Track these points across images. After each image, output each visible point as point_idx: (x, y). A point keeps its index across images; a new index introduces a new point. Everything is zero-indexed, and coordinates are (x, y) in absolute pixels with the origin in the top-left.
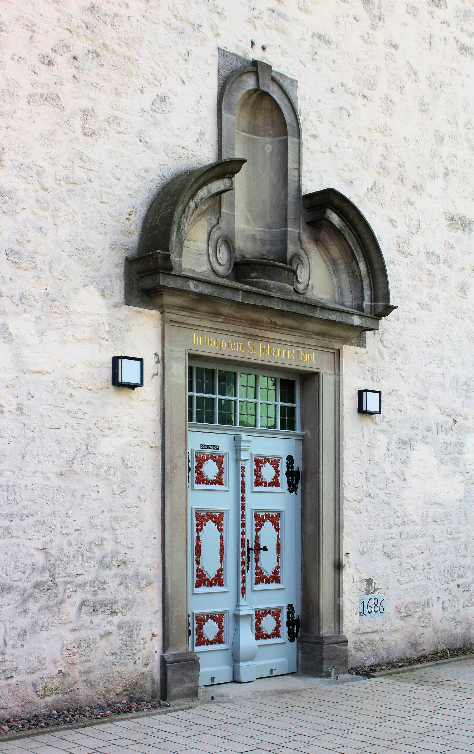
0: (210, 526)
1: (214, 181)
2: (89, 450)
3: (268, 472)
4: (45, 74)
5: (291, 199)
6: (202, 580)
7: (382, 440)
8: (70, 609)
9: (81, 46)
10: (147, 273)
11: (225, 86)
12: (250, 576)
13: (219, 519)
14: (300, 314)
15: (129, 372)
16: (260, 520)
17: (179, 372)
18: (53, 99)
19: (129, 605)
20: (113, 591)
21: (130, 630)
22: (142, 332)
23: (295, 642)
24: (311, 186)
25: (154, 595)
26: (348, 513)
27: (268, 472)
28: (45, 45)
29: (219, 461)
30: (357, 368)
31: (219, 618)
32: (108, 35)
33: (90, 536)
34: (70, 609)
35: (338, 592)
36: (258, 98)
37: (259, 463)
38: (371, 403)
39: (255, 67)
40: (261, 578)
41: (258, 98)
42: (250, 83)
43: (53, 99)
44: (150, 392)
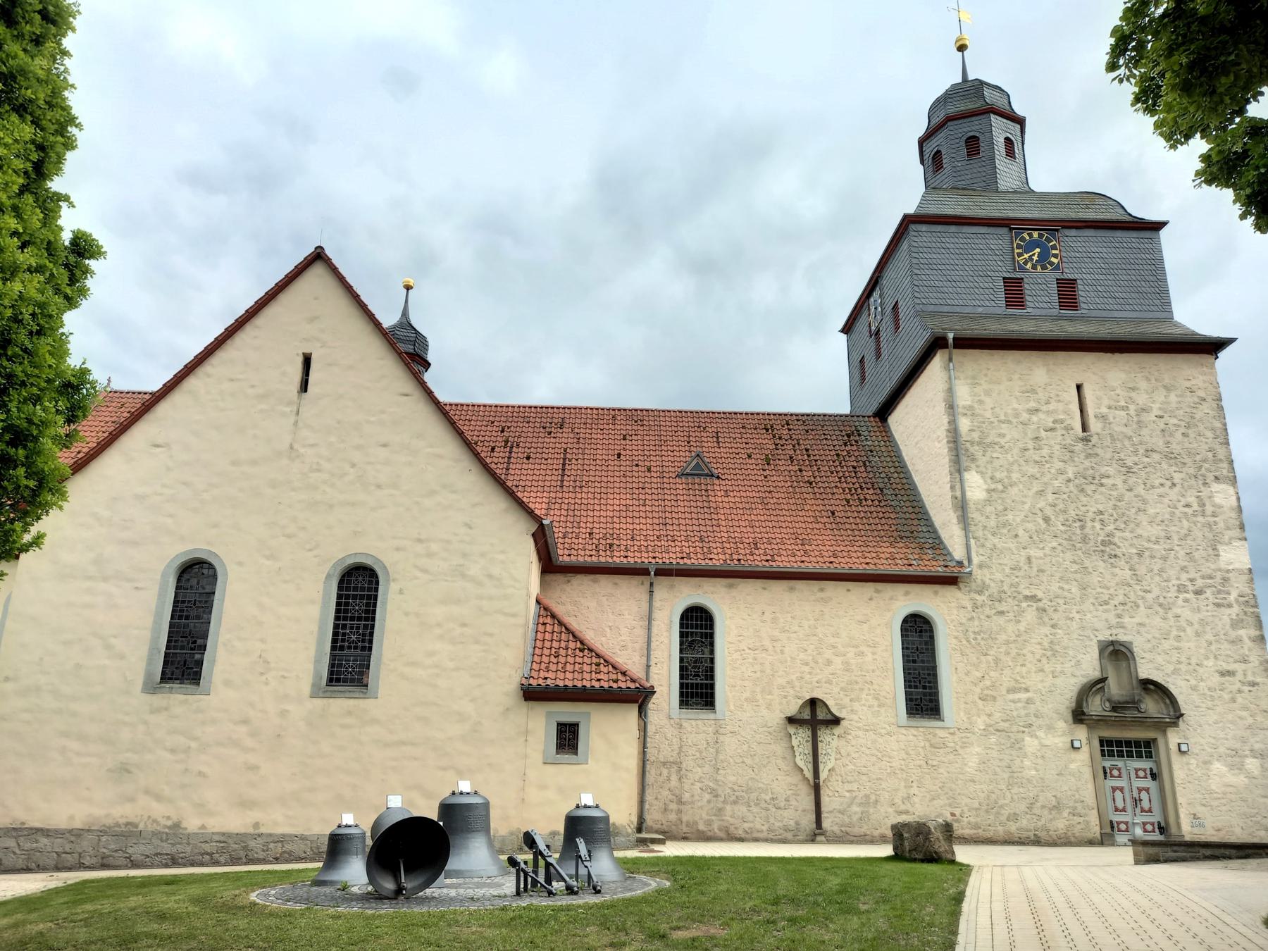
0: (1118, 792)
1: (151, 827)
2: (1066, 767)
3: (1141, 774)
4: (1039, 665)
5: (1134, 682)
6: (1117, 810)
7: (1193, 761)
8: (1065, 814)
9: (1049, 653)
10: (1079, 715)
11: (1101, 652)
12: (1138, 810)
13: (1121, 789)
14: (1142, 722)
15: (1077, 744)
16: (1140, 790)
17: (1096, 743)
18: (1042, 670)
19: (1086, 815)
20: (1080, 809)
21: (1088, 823)
22: (1081, 733)
23: (66, 237)
24: (1143, 675)
25: (1095, 812)
26: (1178, 789)
27: (1141, 774)
28: (1038, 657)
29: (1119, 770)
30: (1173, 737)
31: (1126, 823)
32: (1057, 648)
33: (1069, 793)
34: (1065, 814)
35: (1177, 817)
36: (1116, 652)
37: (1137, 770)
38: (1184, 748)
39: (1112, 643)
40: (1143, 810)
41: (1116, 652)
42: (1111, 648)
43: (1042, 670)
44: (1085, 749)
